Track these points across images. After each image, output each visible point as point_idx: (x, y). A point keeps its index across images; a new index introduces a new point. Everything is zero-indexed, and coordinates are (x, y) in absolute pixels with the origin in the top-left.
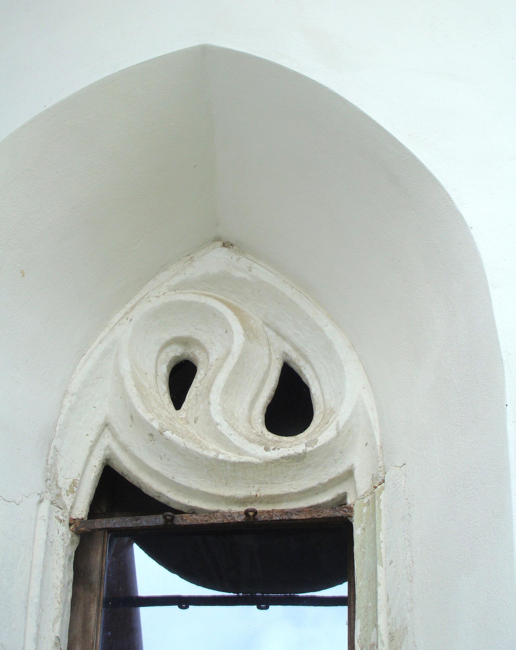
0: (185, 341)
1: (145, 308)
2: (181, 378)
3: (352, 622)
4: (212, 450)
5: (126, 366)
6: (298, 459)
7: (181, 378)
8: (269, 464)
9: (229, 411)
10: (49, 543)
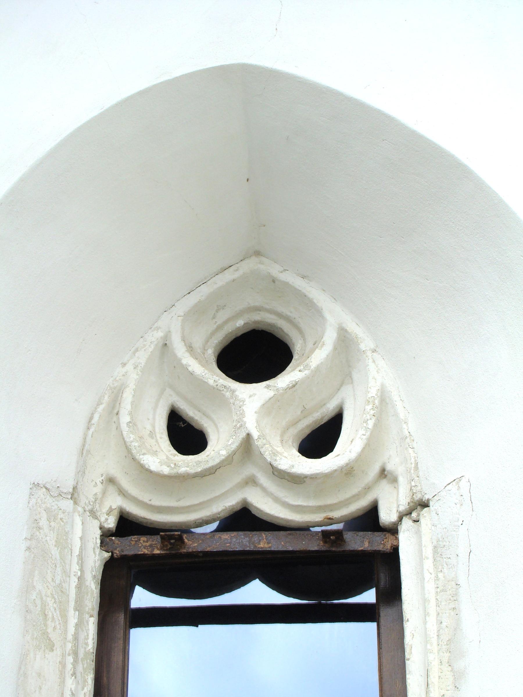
2: (276, 29)
7: (276, 29)
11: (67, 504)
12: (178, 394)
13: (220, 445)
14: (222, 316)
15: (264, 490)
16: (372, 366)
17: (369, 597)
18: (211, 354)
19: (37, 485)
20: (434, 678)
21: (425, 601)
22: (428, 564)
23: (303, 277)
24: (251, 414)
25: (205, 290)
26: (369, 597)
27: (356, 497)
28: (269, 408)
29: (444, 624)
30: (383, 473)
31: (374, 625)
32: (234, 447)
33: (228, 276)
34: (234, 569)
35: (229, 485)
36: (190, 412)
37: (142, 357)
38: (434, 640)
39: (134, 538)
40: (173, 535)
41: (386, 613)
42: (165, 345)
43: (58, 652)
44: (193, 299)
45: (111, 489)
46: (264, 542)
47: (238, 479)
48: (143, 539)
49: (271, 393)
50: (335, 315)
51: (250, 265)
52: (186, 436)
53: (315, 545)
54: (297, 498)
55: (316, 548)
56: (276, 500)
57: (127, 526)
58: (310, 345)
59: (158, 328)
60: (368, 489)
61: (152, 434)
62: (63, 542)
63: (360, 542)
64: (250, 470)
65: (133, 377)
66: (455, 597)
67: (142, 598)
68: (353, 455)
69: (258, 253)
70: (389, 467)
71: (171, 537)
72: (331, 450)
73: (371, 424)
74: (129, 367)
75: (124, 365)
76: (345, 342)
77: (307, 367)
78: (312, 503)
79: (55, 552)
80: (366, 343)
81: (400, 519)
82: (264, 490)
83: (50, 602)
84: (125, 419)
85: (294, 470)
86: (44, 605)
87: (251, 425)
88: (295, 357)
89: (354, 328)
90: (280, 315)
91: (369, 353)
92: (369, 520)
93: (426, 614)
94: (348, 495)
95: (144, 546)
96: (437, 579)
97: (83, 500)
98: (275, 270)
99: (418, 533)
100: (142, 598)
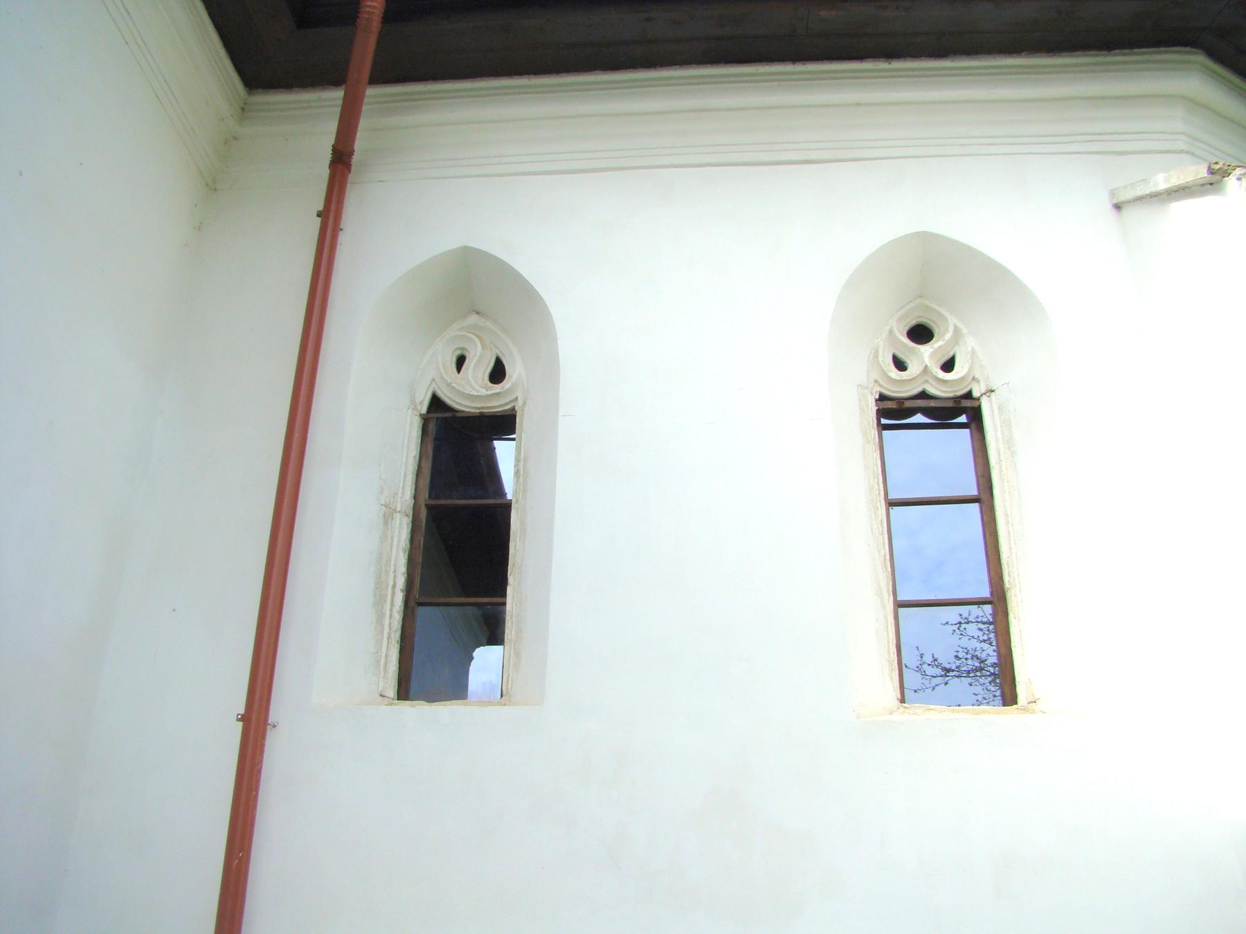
0: (462, 349)
1: (440, 415)
2: (461, 362)
3: (980, 461)
4: (469, 391)
5: (440, 358)
6: (498, 394)
7: (461, 362)
8: (488, 396)
9: (477, 370)
10: (411, 423)
13: (913, 369)
17: (963, 419)
22: (996, 412)
24: (925, 356)
28: (932, 355)
30: (974, 379)
33: (912, 305)
34: (912, 412)
36: (901, 356)
37: (884, 336)
40: (900, 401)
41: (973, 426)
42: (891, 331)
44: (900, 314)
46: (933, 404)
50: (952, 320)
53: (950, 404)
54: (943, 387)
57: (882, 398)
63: (966, 403)
64: (926, 377)
65: (882, 343)
67: (884, 421)
76: (957, 331)
80: (965, 331)
87: (927, 361)
92: (969, 395)
98: (928, 303)
100: (884, 421)
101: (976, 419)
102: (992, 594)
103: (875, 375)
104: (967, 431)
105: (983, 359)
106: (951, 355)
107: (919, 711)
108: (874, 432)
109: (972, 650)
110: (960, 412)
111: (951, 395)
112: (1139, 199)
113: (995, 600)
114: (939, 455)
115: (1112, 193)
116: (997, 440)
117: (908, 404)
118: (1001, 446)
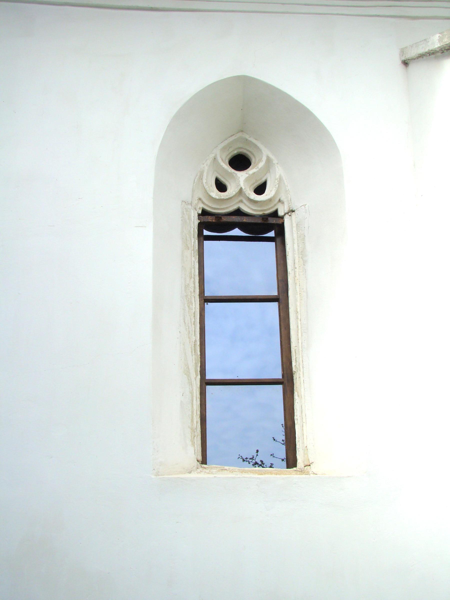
11: (189, 207)
12: (218, 173)
13: (231, 191)
14: (231, 150)
15: (245, 204)
16: (277, 169)
17: (272, 234)
18: (227, 161)
19: (183, 201)
20: (297, 261)
21: (293, 240)
22: (295, 229)
23: (256, 139)
24: (241, 180)
25: (226, 142)
26: (272, 234)
27: (272, 208)
28: (247, 180)
29: (300, 247)
30: (280, 201)
31: (274, 243)
32: (237, 191)
35: (235, 202)
36: (222, 179)
37: (209, 162)
38: (297, 252)
39: (207, 217)
40: (218, 216)
41: (278, 240)
42: (215, 159)
43: (190, 250)
45: (200, 202)
46: (245, 220)
47: (237, 201)
48: (210, 217)
49: (247, 175)
50: (266, 152)
51: (240, 135)
52: (221, 186)
53: (260, 221)
55: (260, 222)
56: (249, 207)
57: (204, 213)
58: (257, 159)
59: (213, 153)
60: (275, 205)
61: (211, 186)
62: (190, 219)
63: (272, 221)
64: (241, 198)
65: (206, 168)
66: (304, 239)
67: (206, 233)
68: (272, 196)
69: (242, 131)
70: (281, 199)
71: (219, 217)
72: (264, 193)
73: (277, 186)
74: (205, 165)
75: (203, 164)
76: (269, 160)
77: (258, 168)
78: (259, 209)
79: (188, 221)
80: (275, 161)
81: (285, 215)
82: (245, 204)
83: (187, 235)
84: (204, 181)
85: (255, 199)
86: (186, 236)
87: (242, 185)
88: (252, 164)
89: (271, 156)
90: (248, 151)
91: (276, 165)
92: (275, 214)
93: (294, 243)
94: (270, 207)
95: (210, 219)
96: (298, 233)
97: (193, 205)
98: (247, 137)
99: (291, 220)
100: (206, 233)
101: (280, 231)
102: (283, 376)
103: (199, 194)
104: (273, 244)
105: (288, 185)
106: (263, 180)
107: (214, 471)
108: (195, 242)
109: (254, 407)
110: (266, 228)
111: (261, 213)
112: (421, 56)
113: (286, 382)
114: (242, 264)
115: (402, 52)
116: (294, 250)
117: (225, 219)
118: (296, 256)
